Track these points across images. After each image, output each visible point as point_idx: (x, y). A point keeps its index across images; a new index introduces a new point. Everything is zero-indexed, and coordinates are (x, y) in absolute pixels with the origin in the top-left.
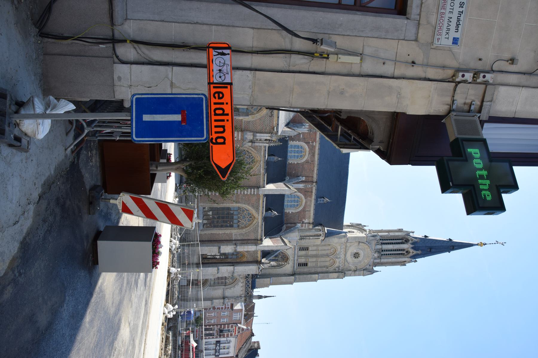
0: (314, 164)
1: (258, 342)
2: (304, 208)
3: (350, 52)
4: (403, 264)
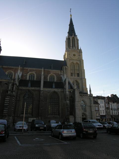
0: (37, 70)
1: (111, 95)
2: (54, 74)
4: (78, 40)
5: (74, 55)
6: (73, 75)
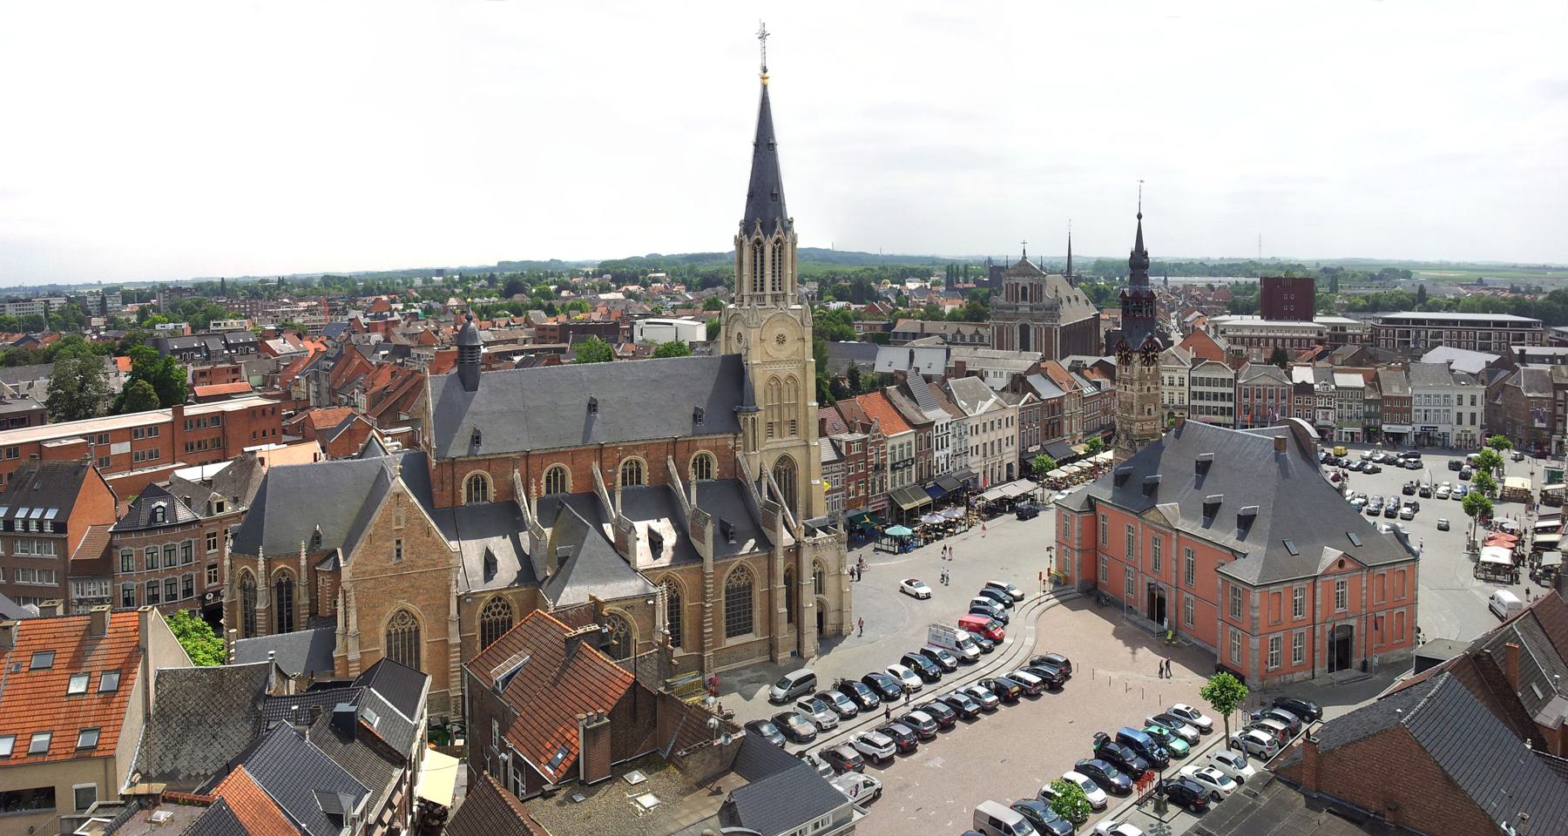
3: (796, 605)
5: (781, 340)
6: (776, 430)
